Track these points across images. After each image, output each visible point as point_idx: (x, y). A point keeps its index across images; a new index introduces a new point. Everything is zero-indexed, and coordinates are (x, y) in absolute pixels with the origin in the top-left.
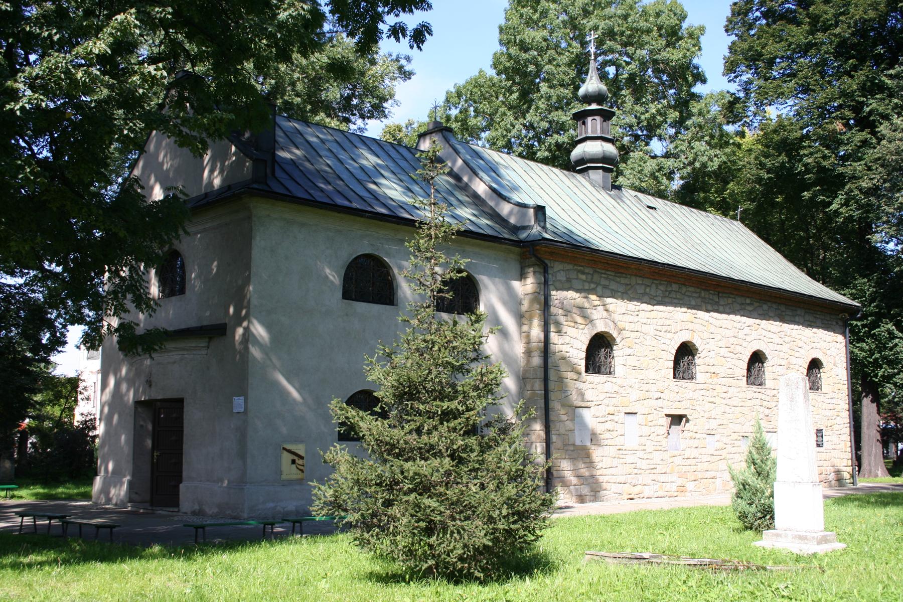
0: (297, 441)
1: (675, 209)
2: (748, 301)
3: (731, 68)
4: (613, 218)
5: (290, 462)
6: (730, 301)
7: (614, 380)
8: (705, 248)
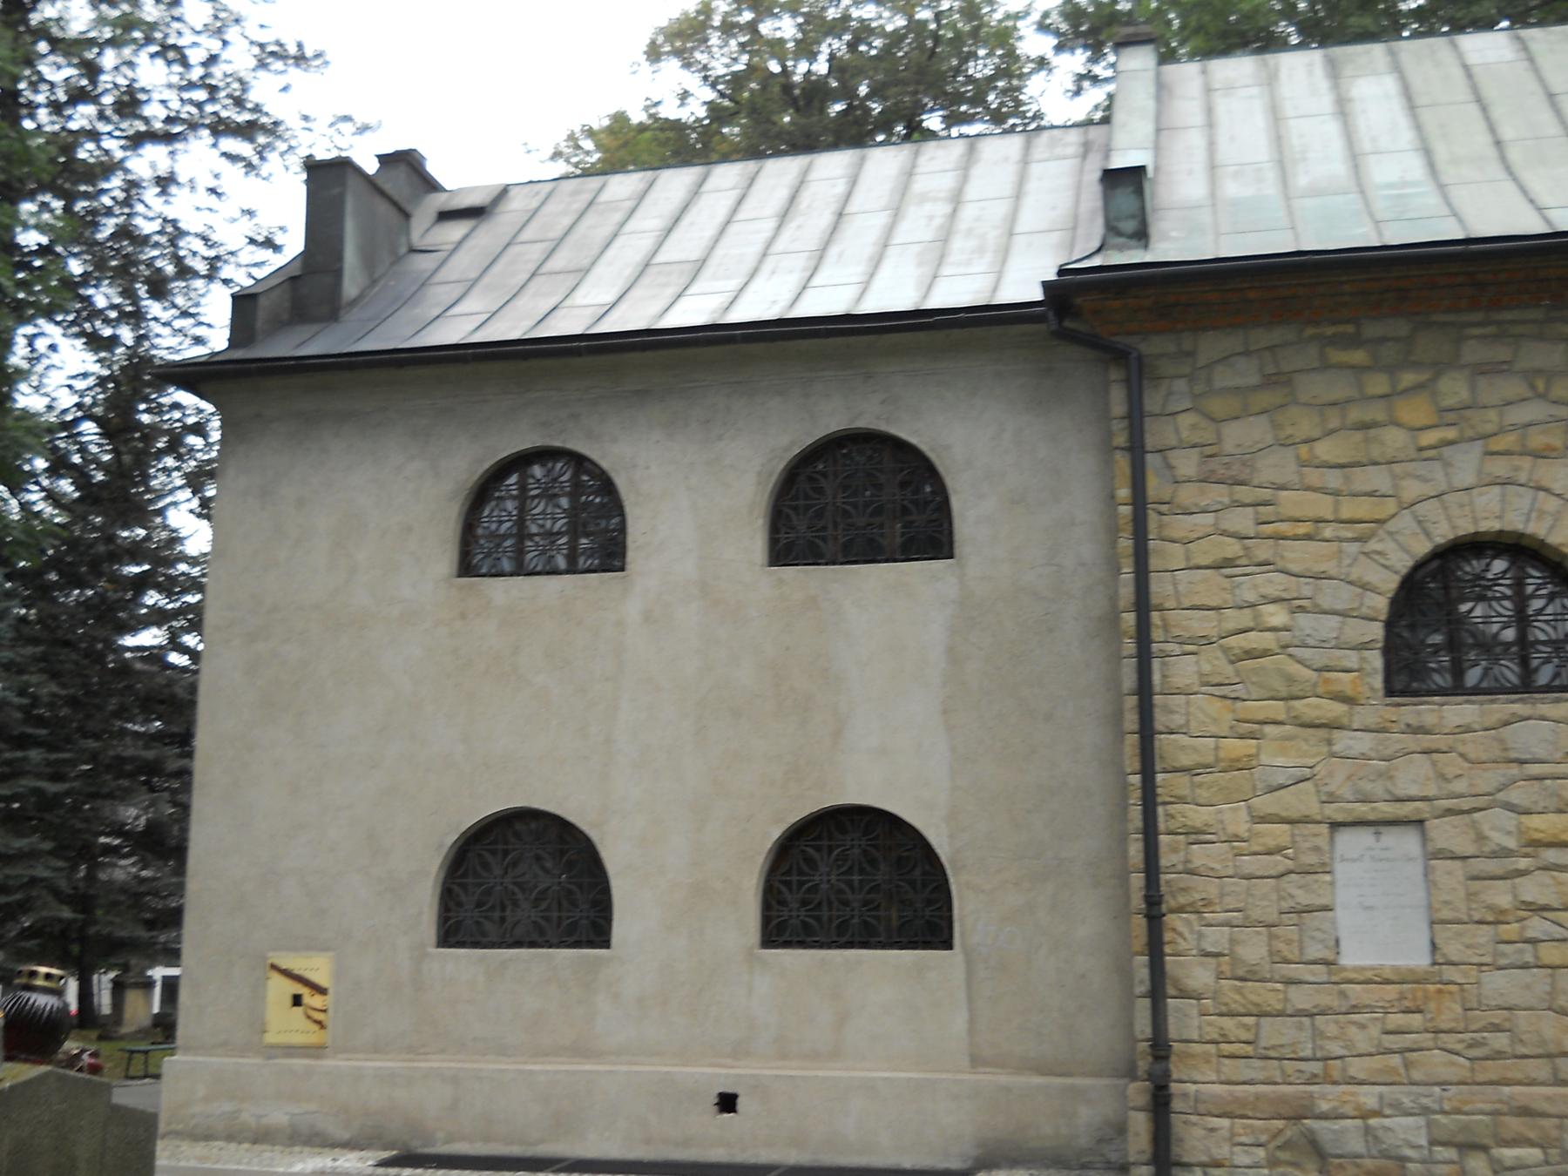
0: (313, 945)
5: (289, 1001)
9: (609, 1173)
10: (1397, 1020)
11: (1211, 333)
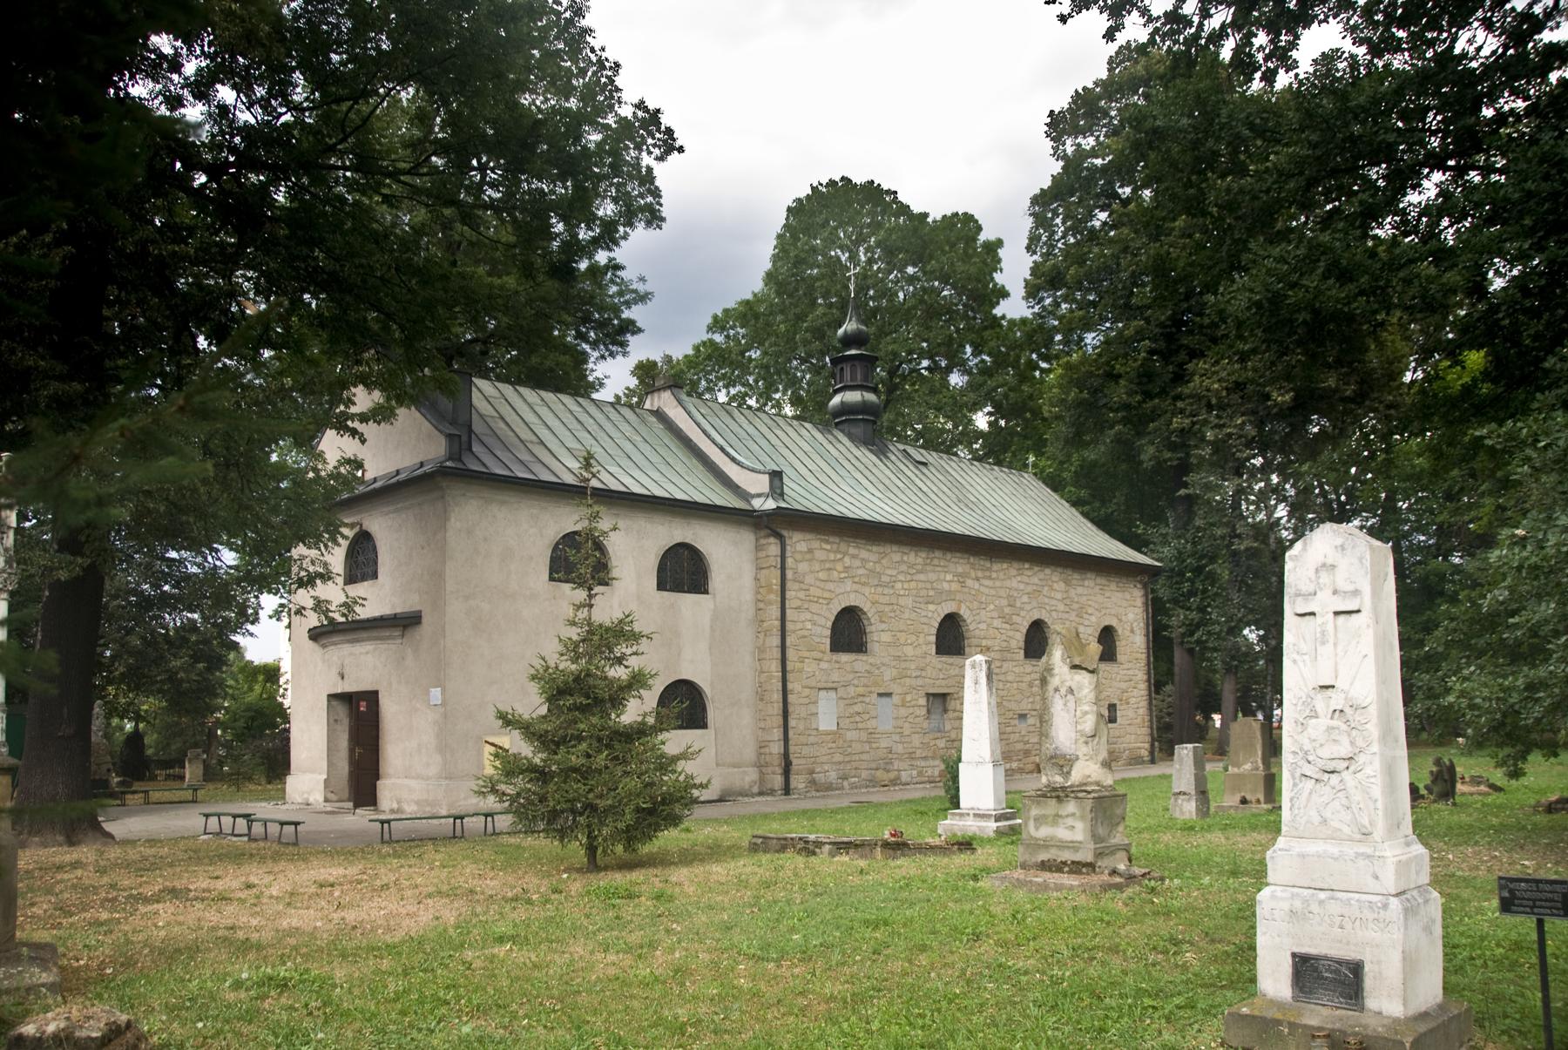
1: (953, 464)
2: (1027, 566)
3: (1032, 292)
4: (872, 478)
6: (1005, 566)
7: (865, 658)
8: (981, 507)
9: (9, 731)
10: (830, 745)
11: (474, 502)
